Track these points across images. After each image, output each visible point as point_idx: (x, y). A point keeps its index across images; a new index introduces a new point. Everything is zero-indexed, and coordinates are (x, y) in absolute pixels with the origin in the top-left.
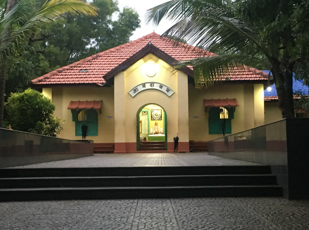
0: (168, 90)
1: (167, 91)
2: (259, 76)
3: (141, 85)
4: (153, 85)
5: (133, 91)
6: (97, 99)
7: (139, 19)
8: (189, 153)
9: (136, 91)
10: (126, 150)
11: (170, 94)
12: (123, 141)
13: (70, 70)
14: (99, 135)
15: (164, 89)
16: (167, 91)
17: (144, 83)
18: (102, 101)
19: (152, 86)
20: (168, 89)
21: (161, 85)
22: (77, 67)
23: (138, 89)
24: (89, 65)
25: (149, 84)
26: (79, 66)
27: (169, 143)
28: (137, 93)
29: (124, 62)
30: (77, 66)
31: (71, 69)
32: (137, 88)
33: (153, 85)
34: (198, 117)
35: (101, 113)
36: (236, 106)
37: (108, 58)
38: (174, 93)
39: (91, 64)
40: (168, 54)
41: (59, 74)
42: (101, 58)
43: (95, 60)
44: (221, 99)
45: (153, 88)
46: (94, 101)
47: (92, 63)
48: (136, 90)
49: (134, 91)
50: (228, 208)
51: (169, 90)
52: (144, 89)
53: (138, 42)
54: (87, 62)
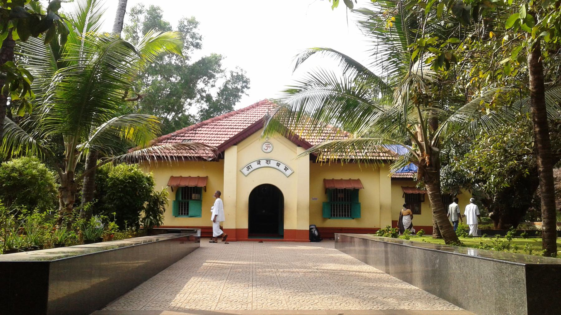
0: (286, 169)
1: (285, 169)
2: (387, 155)
3: (256, 162)
4: (269, 162)
5: (246, 169)
6: (202, 174)
7: (144, 21)
8: (309, 243)
9: (250, 168)
10: (236, 237)
11: (288, 172)
12: (233, 227)
13: (170, 139)
14: (202, 215)
15: (282, 167)
16: (285, 169)
17: (259, 160)
18: (207, 177)
19: (268, 164)
20: (286, 168)
21: (279, 162)
22: (179, 136)
23: (252, 166)
24: (194, 134)
25: (265, 161)
26: (182, 135)
27: (286, 230)
28: (250, 170)
29: (235, 136)
30: (179, 135)
31: (172, 138)
32: (250, 166)
33: (269, 162)
34: (316, 199)
35: (206, 191)
36: (361, 188)
37: (215, 127)
38: (294, 172)
39: (195, 134)
40: (309, 143)
41: (158, 144)
42: (206, 126)
43: (200, 129)
44: (344, 179)
45: (269, 165)
46: (198, 177)
47: (197, 132)
48: (250, 167)
49: (247, 169)
50: (319, 283)
51: (288, 169)
52: (259, 166)
53: (249, 110)
54: (191, 130)
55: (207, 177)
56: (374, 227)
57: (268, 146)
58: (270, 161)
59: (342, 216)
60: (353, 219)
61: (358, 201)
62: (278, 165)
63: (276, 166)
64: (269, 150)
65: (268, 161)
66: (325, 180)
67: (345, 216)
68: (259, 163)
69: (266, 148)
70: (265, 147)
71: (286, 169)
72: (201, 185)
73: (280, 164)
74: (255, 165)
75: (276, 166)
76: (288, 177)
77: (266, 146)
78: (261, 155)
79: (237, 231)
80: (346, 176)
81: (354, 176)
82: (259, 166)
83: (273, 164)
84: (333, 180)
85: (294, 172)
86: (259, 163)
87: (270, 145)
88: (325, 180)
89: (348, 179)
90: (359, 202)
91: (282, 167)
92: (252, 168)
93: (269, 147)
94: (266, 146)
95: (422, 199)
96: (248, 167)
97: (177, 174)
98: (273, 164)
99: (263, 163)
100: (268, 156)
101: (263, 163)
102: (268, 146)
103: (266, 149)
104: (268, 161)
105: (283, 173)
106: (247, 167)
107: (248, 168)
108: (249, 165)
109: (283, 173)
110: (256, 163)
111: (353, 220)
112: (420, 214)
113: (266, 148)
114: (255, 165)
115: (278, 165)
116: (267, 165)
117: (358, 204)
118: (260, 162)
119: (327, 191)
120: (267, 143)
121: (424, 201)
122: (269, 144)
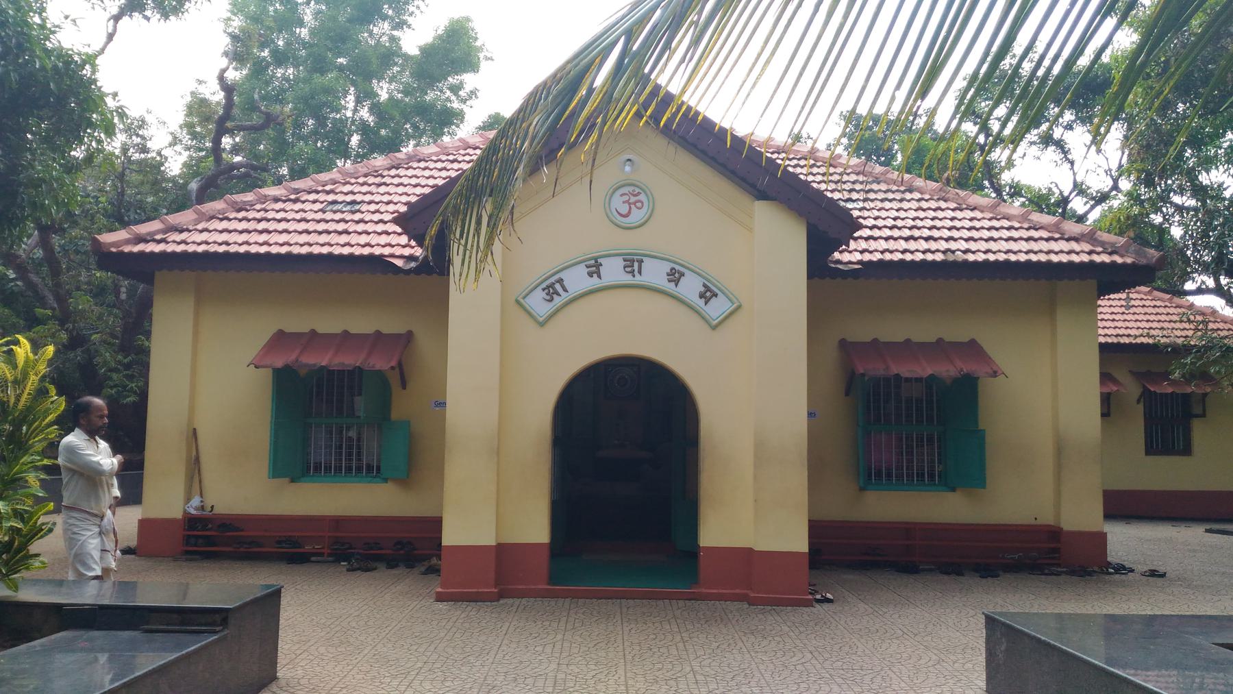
0: (708, 294)
1: (702, 296)
3: (583, 265)
4: (636, 264)
5: (539, 294)
6: (391, 324)
11: (716, 309)
15: (690, 287)
16: (702, 296)
19: (632, 272)
20: (707, 289)
21: (677, 267)
25: (619, 262)
27: (703, 547)
32: (560, 281)
33: (636, 264)
38: (739, 307)
45: (638, 279)
48: (558, 286)
49: (543, 294)
52: (594, 282)
55: (409, 335)
56: (1033, 522)
57: (633, 199)
58: (640, 262)
59: (899, 477)
60: (953, 490)
61: (976, 422)
62: (675, 276)
63: (662, 282)
64: (637, 216)
65: (633, 263)
66: (843, 344)
67: (921, 476)
68: (595, 268)
69: (624, 209)
70: (618, 203)
71: (708, 294)
72: (380, 363)
73: (682, 275)
74: (577, 280)
75: (662, 282)
76: (714, 328)
77: (626, 198)
78: (603, 238)
79: (503, 552)
80: (924, 330)
81: (957, 330)
82: (594, 282)
83: (654, 273)
84: (875, 347)
85: (739, 307)
86: (595, 268)
87: (642, 197)
88: (843, 344)
89: (932, 339)
90: (981, 427)
91: (690, 287)
92: (566, 291)
93: (638, 204)
94: (626, 198)
95: (1197, 410)
96: (552, 286)
97: (299, 321)
98: (654, 273)
99: (613, 271)
100: (633, 242)
101: (613, 271)
102: (633, 199)
103: (624, 212)
104: (633, 263)
105: (698, 312)
106: (544, 285)
107: (551, 292)
108: (552, 280)
109: (698, 312)
110: (582, 270)
111: (950, 495)
112: (1148, 453)
113: (624, 209)
114: (577, 280)
115: (675, 276)
116: (627, 279)
117: (978, 437)
118: (598, 266)
119: (851, 382)
120: (631, 189)
121: (1204, 415)
122: (637, 190)
